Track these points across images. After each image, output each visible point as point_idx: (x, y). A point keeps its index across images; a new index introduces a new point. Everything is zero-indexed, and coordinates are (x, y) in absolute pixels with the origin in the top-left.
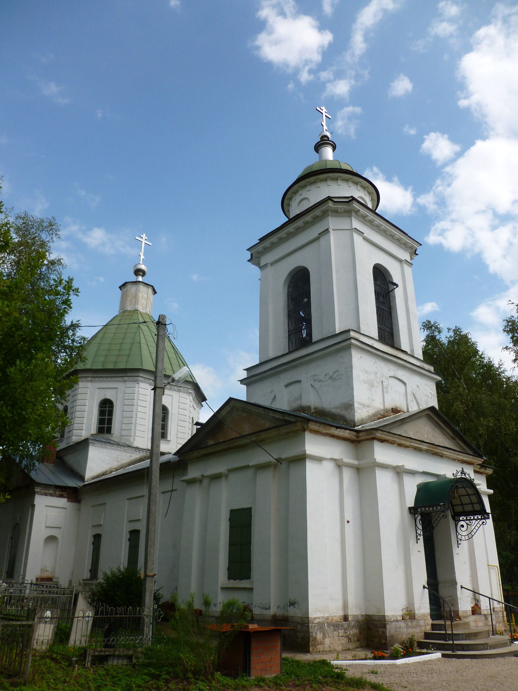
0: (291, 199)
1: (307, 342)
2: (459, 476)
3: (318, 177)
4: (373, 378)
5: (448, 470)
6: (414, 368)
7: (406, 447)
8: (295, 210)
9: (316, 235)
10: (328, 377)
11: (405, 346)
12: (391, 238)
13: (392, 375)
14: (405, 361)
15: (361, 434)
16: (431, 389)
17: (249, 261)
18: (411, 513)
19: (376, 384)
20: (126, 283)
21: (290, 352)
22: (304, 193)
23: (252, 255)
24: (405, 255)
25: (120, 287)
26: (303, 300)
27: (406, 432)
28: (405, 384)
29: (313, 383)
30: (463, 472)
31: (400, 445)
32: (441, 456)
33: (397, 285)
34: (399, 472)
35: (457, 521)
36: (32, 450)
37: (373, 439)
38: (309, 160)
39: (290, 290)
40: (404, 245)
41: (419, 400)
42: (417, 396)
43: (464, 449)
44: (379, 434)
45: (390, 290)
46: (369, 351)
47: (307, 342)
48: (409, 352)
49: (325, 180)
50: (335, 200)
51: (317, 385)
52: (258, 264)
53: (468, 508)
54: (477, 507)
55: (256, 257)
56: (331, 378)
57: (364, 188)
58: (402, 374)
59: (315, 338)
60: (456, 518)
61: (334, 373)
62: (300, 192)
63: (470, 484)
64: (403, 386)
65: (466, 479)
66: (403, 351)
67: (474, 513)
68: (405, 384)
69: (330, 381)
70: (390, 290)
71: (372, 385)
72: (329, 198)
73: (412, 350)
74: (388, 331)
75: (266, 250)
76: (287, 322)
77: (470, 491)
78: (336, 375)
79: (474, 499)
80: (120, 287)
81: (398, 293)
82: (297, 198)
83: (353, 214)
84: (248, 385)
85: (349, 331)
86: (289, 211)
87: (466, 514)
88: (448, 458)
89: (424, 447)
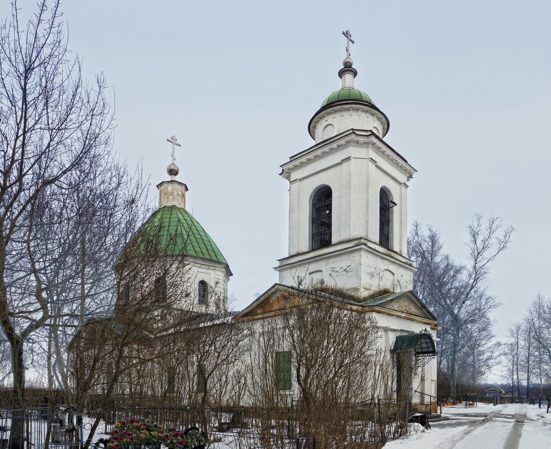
0: (317, 122)
1: (328, 243)
2: (423, 332)
3: (343, 106)
4: (374, 271)
5: (417, 328)
6: (401, 263)
7: (392, 315)
8: (321, 135)
9: (339, 161)
10: (342, 270)
11: (396, 248)
12: (395, 166)
13: (386, 268)
14: (396, 259)
15: (365, 308)
16: (410, 278)
17: (280, 174)
18: (391, 353)
19: (375, 275)
20: (163, 182)
21: (313, 250)
22: (330, 119)
23: (283, 170)
24: (402, 178)
25: (157, 186)
26: (325, 211)
27: (393, 306)
28: (393, 274)
29: (331, 273)
30: (426, 330)
31: (389, 314)
32: (412, 320)
33: (396, 204)
34: (386, 330)
35: (417, 357)
36: (69, 271)
37: (373, 311)
38: (335, 86)
39: (315, 202)
40: (401, 169)
41: (401, 285)
42: (400, 282)
43: (426, 316)
44: (377, 308)
45: (390, 206)
46: (373, 253)
47: (328, 243)
48: (398, 252)
49: (349, 109)
50: (358, 133)
51: (334, 274)
52: (288, 178)
53: (424, 350)
54: (431, 349)
55: (287, 173)
56: (345, 270)
57: (379, 119)
58: (392, 268)
59: (334, 240)
60: (417, 355)
61: (348, 267)
62: (326, 118)
63: (429, 337)
64: (392, 275)
65: (427, 334)
66: (395, 252)
67: (428, 352)
68: (393, 274)
69: (344, 272)
70: (390, 206)
71: (373, 276)
72: (354, 131)
73: (401, 251)
74: (385, 239)
75: (296, 168)
76: (311, 226)
77: (428, 341)
78: (348, 268)
79: (430, 345)
80: (157, 186)
81: (396, 209)
82: (323, 123)
83: (370, 146)
84: (280, 271)
85: (361, 238)
86: (314, 132)
87: (423, 353)
88: (417, 321)
89: (403, 315)
